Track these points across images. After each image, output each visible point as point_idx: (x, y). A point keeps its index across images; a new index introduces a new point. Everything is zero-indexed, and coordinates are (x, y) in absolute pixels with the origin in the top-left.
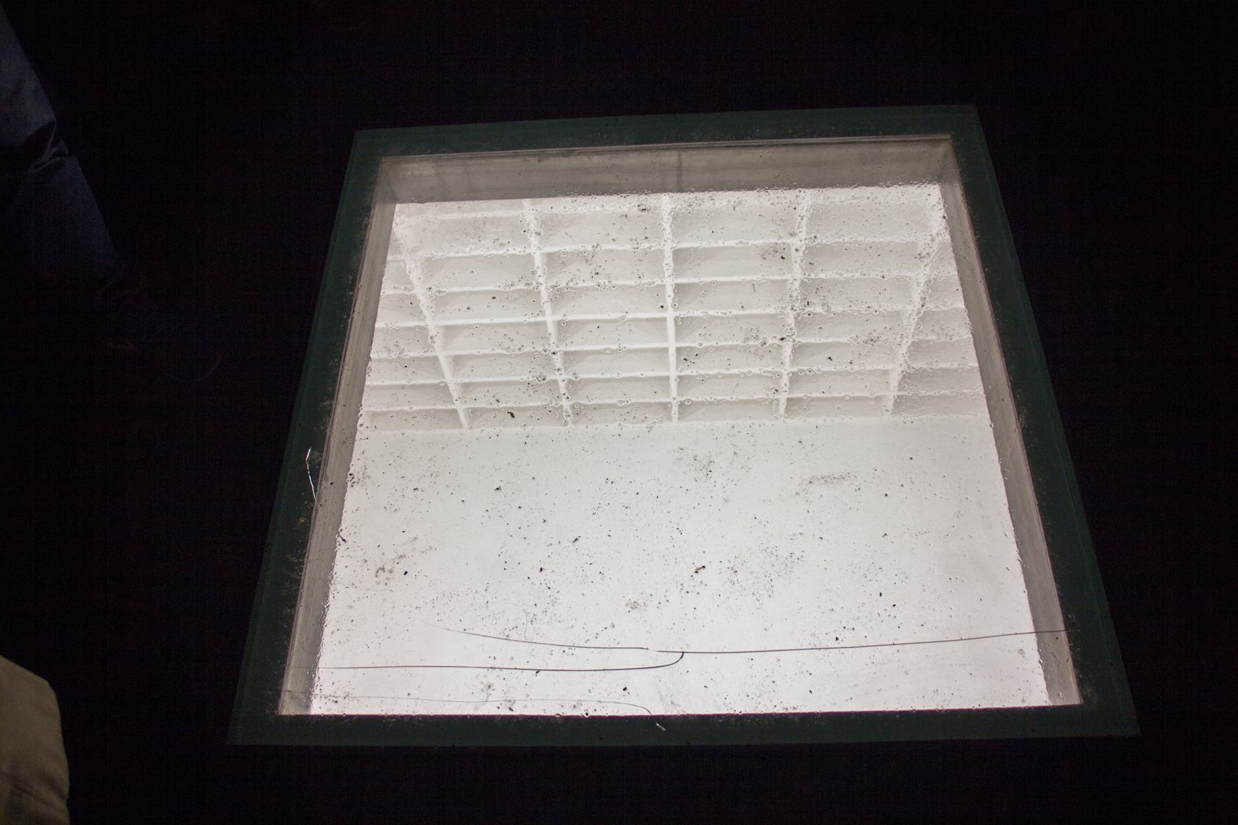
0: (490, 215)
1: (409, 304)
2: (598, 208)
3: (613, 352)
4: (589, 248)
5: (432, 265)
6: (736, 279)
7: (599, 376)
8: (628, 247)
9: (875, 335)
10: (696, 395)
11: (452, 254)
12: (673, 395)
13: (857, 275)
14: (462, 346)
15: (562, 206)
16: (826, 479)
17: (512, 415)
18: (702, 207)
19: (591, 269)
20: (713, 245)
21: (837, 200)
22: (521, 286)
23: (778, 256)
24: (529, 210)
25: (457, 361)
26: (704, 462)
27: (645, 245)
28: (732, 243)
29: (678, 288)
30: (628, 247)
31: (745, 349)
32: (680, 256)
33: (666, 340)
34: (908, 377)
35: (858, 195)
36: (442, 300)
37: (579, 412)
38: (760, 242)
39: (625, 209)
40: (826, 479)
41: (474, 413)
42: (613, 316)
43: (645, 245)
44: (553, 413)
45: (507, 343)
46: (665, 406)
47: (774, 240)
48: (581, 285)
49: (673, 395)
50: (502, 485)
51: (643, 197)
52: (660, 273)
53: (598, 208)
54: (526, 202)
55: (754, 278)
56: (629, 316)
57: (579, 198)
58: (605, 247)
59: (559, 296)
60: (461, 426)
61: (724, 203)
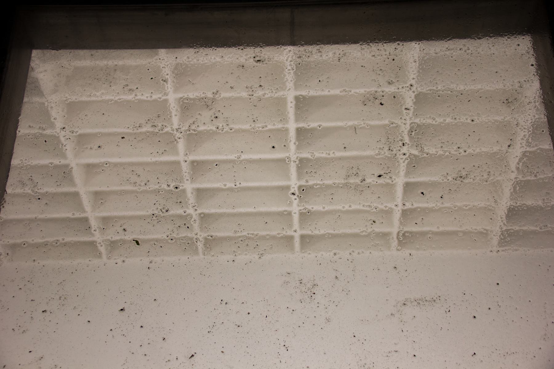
0: (121, 63)
1: (52, 144)
2: (218, 59)
3: (231, 190)
4: (210, 95)
5: (72, 108)
6: (340, 124)
7: (230, 211)
8: (244, 94)
9: (464, 174)
10: (320, 228)
11: (84, 99)
12: (296, 230)
13: (448, 120)
14: (101, 183)
15: (188, 56)
16: (418, 302)
17: (138, 243)
18: (311, 59)
19: (211, 113)
20: (320, 93)
21: (432, 52)
22: (147, 128)
23: (378, 102)
24: (165, 59)
25: (99, 197)
26: (309, 285)
27: (260, 93)
28: (337, 92)
29: (299, 131)
30: (244, 94)
31: (346, 186)
32: (301, 103)
33: (289, 179)
34: (513, 213)
35: (451, 47)
36: (82, 140)
37: (210, 243)
38: (362, 91)
39: (242, 60)
40: (418, 302)
41: (113, 245)
42: (232, 157)
43: (260, 93)
44: (189, 245)
45: (134, 178)
46: (290, 239)
47: (373, 89)
48: (202, 128)
49: (296, 230)
50: (126, 306)
51: (258, 50)
52: (284, 119)
53: (218, 59)
54: (162, 52)
55: (356, 123)
56: (243, 157)
57: (201, 50)
58: (224, 95)
59: (195, 138)
60: (100, 255)
61: (331, 54)
